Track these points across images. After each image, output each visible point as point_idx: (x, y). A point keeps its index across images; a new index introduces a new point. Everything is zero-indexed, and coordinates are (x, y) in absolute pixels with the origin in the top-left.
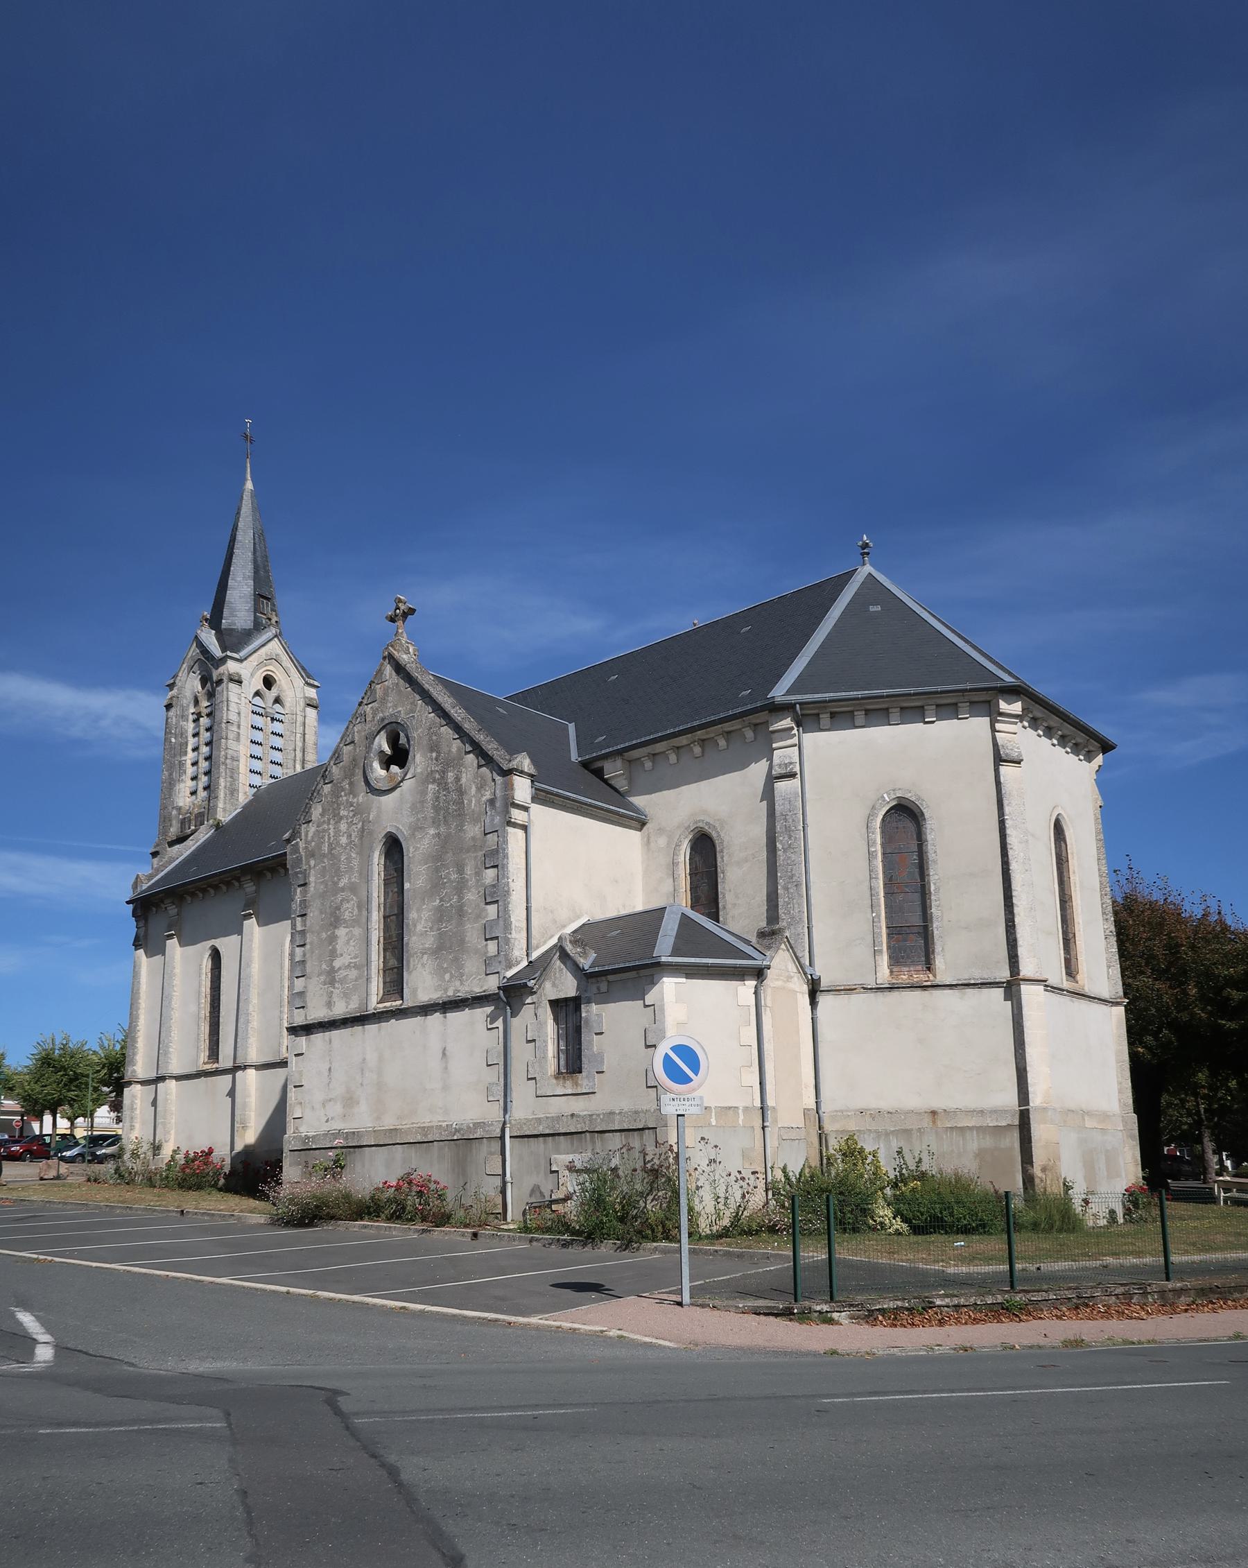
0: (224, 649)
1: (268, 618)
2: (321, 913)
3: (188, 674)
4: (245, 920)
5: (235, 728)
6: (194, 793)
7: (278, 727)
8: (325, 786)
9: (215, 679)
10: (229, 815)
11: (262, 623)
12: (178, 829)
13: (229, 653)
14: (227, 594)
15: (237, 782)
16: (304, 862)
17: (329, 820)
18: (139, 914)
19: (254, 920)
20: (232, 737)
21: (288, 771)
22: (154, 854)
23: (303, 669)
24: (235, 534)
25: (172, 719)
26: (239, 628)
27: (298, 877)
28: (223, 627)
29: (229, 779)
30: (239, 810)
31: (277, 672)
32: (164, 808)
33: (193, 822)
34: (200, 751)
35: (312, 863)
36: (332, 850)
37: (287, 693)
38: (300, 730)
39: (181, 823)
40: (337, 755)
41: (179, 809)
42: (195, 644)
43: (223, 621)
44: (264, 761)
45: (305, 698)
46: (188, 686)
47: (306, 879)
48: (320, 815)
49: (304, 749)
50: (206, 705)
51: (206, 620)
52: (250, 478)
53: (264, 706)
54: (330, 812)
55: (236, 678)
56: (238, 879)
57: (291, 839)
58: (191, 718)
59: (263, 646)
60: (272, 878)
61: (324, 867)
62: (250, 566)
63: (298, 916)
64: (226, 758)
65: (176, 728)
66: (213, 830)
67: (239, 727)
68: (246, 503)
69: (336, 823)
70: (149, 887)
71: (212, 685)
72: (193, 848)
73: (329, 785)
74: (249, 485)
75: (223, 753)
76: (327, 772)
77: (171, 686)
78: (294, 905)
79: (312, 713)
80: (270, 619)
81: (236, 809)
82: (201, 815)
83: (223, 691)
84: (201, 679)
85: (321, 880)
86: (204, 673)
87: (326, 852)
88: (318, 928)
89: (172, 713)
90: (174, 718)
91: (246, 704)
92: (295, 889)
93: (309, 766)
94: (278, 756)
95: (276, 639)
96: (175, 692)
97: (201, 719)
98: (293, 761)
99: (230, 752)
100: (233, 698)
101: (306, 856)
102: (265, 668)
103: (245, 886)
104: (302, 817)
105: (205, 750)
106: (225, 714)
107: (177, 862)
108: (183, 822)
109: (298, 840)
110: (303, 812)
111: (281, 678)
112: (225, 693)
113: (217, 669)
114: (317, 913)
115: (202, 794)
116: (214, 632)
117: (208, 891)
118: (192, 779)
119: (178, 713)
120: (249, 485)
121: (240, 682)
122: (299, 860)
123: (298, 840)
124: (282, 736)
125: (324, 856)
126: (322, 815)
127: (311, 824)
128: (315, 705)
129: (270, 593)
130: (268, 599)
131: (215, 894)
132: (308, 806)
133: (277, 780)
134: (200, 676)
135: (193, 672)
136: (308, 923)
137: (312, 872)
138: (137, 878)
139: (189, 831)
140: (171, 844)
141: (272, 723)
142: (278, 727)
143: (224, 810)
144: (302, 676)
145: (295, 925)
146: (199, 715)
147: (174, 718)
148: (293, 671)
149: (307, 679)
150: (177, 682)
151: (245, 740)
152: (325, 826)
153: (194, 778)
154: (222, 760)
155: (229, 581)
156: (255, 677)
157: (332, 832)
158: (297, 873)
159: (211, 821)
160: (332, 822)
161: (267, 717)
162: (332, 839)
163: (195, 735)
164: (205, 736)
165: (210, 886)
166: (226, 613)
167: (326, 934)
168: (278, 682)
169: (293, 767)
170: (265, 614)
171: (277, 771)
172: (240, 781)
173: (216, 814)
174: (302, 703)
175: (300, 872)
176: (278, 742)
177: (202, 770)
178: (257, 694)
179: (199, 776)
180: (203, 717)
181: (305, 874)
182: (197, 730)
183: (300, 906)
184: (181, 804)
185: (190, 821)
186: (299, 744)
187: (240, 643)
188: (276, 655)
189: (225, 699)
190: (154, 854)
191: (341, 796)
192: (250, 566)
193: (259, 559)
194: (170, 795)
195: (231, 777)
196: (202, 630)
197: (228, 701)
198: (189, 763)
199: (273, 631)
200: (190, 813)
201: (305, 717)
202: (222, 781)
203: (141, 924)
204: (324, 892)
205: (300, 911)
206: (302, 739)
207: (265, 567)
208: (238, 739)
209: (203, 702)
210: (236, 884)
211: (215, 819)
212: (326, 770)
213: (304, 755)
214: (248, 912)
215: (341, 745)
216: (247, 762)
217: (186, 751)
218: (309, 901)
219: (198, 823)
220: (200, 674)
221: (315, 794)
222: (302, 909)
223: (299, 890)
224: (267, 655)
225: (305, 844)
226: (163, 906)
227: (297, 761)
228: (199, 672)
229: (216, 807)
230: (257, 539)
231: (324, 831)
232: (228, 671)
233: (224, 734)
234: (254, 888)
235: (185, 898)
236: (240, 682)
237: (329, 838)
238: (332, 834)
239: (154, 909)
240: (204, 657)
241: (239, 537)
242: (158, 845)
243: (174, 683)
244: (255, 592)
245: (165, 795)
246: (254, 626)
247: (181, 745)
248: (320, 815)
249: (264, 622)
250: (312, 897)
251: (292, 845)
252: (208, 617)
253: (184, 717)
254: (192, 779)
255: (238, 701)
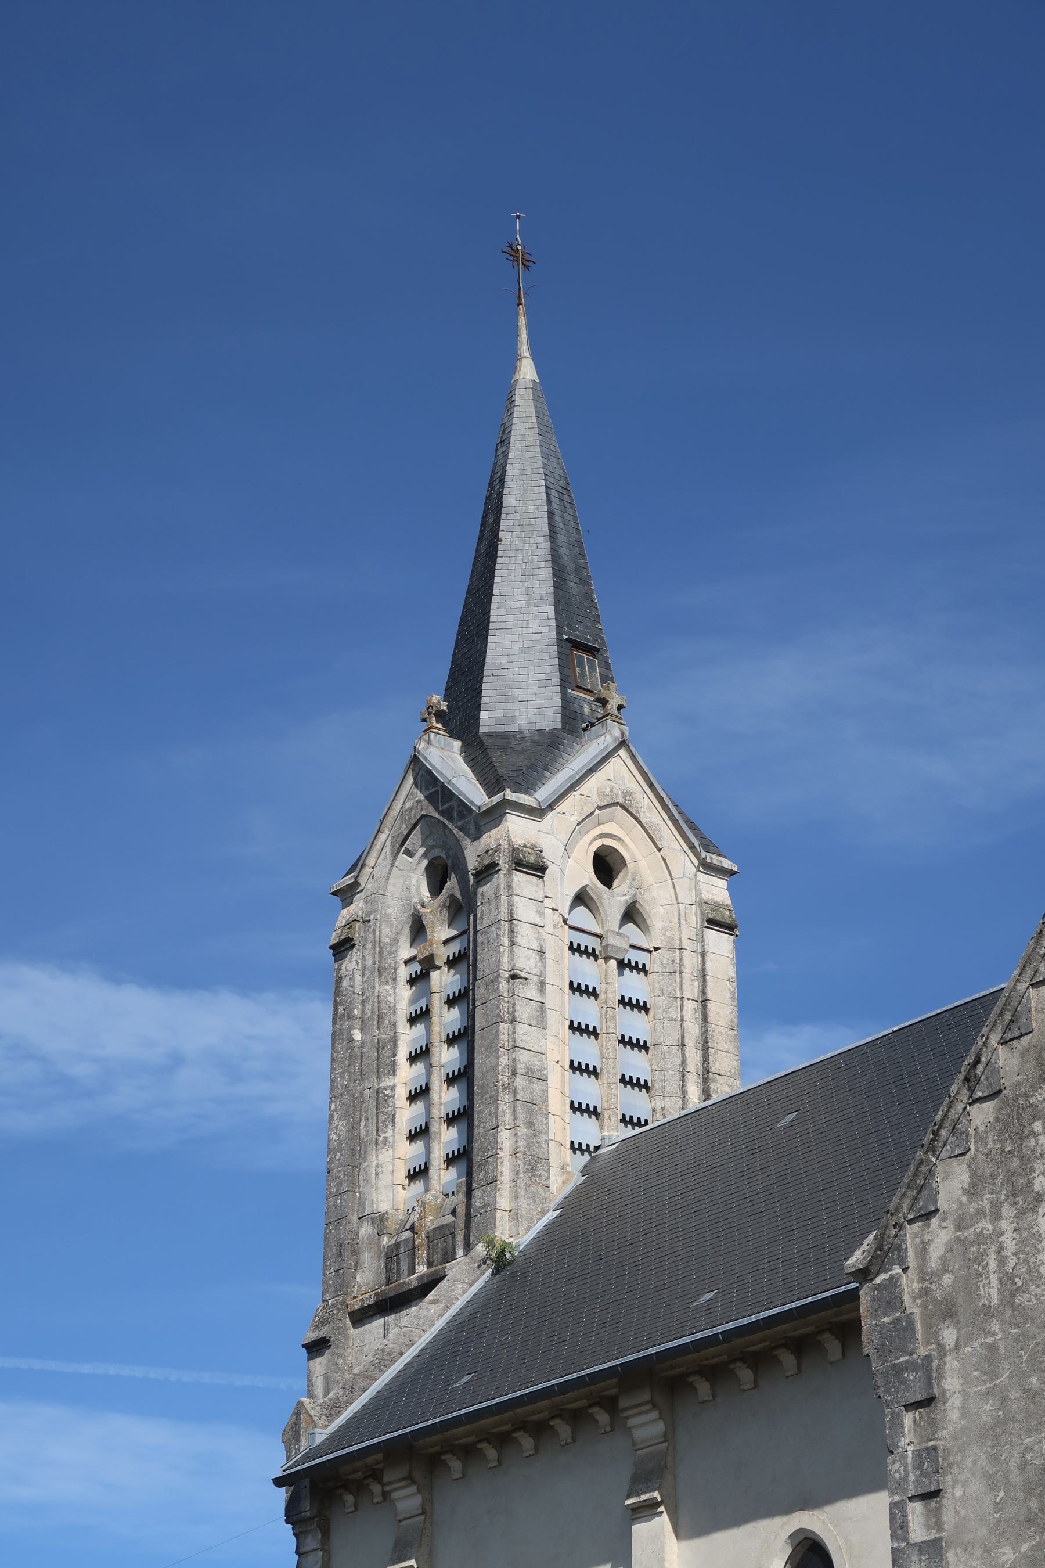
0: (492, 783)
1: (598, 700)
2: (992, 1486)
3: (395, 857)
4: (634, 1520)
5: (532, 992)
6: (419, 1174)
7: (634, 986)
8: (974, 1110)
9: (472, 863)
10: (528, 1229)
11: (582, 714)
12: (378, 1275)
13: (509, 795)
14: (490, 646)
15: (544, 1138)
16: (920, 1334)
17: (997, 1206)
18: (308, 1514)
19: (663, 1522)
20: (525, 1016)
21: (668, 1103)
22: (316, 1348)
23: (693, 828)
24: (500, 495)
25: (352, 979)
26: (526, 730)
27: (904, 1381)
28: (482, 729)
29: (523, 1131)
30: (551, 1215)
31: (627, 840)
32: (337, 1219)
33: (423, 1254)
34: (435, 1059)
35: (949, 1335)
36: (1013, 1295)
37: (655, 893)
38: (692, 989)
39: (389, 1258)
40: (1008, 1016)
41: (380, 1220)
42: (410, 780)
43: (483, 715)
44: (604, 1078)
45: (702, 903)
46: (394, 889)
47: (930, 1385)
48: (965, 1192)
49: (706, 1042)
50: (444, 937)
51: (440, 715)
52: (527, 354)
53: (599, 931)
54: (998, 1182)
55: (532, 859)
56: (611, 1404)
57: (874, 1269)
58: (404, 973)
59: (592, 770)
60: (714, 1396)
61: (993, 1348)
62: (542, 571)
63: (911, 1499)
64: (514, 1073)
65: (363, 1002)
66: (489, 1273)
67: (542, 986)
68: (523, 414)
69: (1022, 1214)
70: (333, 1437)
71: (463, 881)
72: (440, 1324)
73: (989, 1106)
74: (527, 371)
75: (504, 1061)
76: (980, 1068)
77: (346, 894)
78: (897, 1466)
79: (720, 944)
80: (603, 702)
81: (544, 1213)
82: (445, 1232)
83: (497, 896)
84: (427, 868)
85: (983, 1388)
86: (436, 852)
87: (995, 1301)
88: (983, 1531)
89: (351, 963)
90: (358, 978)
91: (555, 926)
92: (897, 1418)
93: (723, 1089)
94: (637, 1064)
95: (622, 752)
96: (357, 907)
97: (434, 975)
98: (678, 1076)
99: (523, 1056)
100: (525, 911)
101: (927, 1317)
102: (598, 831)
103: (631, 1422)
104: (906, 1204)
105: (448, 1057)
106: (506, 954)
107: (399, 1365)
108: (391, 1256)
109: (897, 1270)
110: (909, 1187)
111: (638, 856)
112: (503, 898)
113: (476, 838)
114: (977, 1486)
115: (444, 1177)
116: (457, 744)
117: (552, 1427)
118: (412, 1137)
119: (369, 963)
120: (527, 371)
121: (539, 869)
122: (904, 1329)
123: (897, 1270)
124: (645, 1008)
125: (988, 1312)
126: (973, 1191)
127: (934, 1221)
128: (729, 921)
129: (597, 635)
130: (592, 651)
131: (537, 1450)
132: (924, 1168)
133: (638, 1130)
134: (425, 862)
135: (409, 853)
136: (948, 1518)
137: (952, 1364)
138: (297, 1414)
139: (412, 1281)
140: (360, 1317)
141: (620, 974)
142: (634, 986)
143: (514, 1215)
144: (692, 847)
145: (904, 1526)
146: (428, 964)
147: (358, 978)
148: (668, 834)
149: (704, 854)
150: (362, 880)
151: (557, 1024)
152: (986, 1225)
153: (420, 1133)
154: (503, 1078)
155: (492, 612)
156: (575, 854)
157: (1009, 1242)
158: (898, 1370)
159: (480, 1249)
160: (1007, 1211)
161: (607, 959)
162: (1012, 1261)
163: (417, 1018)
164: (448, 1019)
165: (523, 1426)
166: (488, 692)
167: (1015, 1548)
168: (630, 865)
169: (680, 1093)
170: (590, 691)
171: (638, 1104)
172: (551, 1137)
173: (493, 1227)
174: (694, 919)
175: (912, 1366)
176: (637, 1026)
177: (439, 1112)
178: (581, 899)
179: (434, 1128)
180: (439, 968)
181: (928, 1370)
182: (423, 1003)
183: (919, 1465)
184: (384, 1207)
185: (413, 1250)
186: (693, 1030)
187: (532, 767)
188: (626, 794)
189: (504, 915)
190: (316, 1348)
191: (1032, 1133)
192: (544, 572)
193: (564, 551)
194: (354, 1183)
195: (530, 1125)
196: (429, 742)
197: (511, 920)
198: (402, 1093)
199: (608, 735)
200: (412, 1228)
201: (703, 954)
202: (505, 1138)
203: (311, 1543)
204: (999, 1422)
205: (918, 1481)
206: (698, 1015)
207: (579, 569)
208: (540, 1021)
209: (438, 928)
210: (603, 1417)
211: (490, 1244)
212: (978, 1061)
213: (705, 1058)
214: (644, 1497)
215: (1022, 986)
216: (563, 1083)
217: (394, 1064)
218: (947, 1453)
219: (437, 1257)
220: (425, 855)
221: (944, 1133)
222: (922, 1475)
223: (908, 1419)
224: (601, 794)
225: (922, 1280)
226: (376, 1489)
227: (689, 1076)
228: (422, 850)
229: (490, 1209)
230: (555, 501)
231: (981, 1238)
232: (510, 841)
233: (505, 1008)
234: (661, 1427)
235: (444, 1463)
236: (539, 869)
237: (1002, 1262)
238: (1010, 1247)
239: (349, 1499)
240: (437, 809)
241: (511, 500)
242: (324, 1322)
243: (356, 884)
244: (559, 633)
245: (339, 1184)
246: (563, 722)
247: (379, 1046)
248: (965, 1192)
249: (586, 710)
250: (955, 1438)
251: (878, 1287)
252: (444, 705)
253: (383, 971)
254: (412, 1137)
255: (537, 920)
